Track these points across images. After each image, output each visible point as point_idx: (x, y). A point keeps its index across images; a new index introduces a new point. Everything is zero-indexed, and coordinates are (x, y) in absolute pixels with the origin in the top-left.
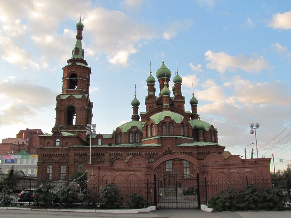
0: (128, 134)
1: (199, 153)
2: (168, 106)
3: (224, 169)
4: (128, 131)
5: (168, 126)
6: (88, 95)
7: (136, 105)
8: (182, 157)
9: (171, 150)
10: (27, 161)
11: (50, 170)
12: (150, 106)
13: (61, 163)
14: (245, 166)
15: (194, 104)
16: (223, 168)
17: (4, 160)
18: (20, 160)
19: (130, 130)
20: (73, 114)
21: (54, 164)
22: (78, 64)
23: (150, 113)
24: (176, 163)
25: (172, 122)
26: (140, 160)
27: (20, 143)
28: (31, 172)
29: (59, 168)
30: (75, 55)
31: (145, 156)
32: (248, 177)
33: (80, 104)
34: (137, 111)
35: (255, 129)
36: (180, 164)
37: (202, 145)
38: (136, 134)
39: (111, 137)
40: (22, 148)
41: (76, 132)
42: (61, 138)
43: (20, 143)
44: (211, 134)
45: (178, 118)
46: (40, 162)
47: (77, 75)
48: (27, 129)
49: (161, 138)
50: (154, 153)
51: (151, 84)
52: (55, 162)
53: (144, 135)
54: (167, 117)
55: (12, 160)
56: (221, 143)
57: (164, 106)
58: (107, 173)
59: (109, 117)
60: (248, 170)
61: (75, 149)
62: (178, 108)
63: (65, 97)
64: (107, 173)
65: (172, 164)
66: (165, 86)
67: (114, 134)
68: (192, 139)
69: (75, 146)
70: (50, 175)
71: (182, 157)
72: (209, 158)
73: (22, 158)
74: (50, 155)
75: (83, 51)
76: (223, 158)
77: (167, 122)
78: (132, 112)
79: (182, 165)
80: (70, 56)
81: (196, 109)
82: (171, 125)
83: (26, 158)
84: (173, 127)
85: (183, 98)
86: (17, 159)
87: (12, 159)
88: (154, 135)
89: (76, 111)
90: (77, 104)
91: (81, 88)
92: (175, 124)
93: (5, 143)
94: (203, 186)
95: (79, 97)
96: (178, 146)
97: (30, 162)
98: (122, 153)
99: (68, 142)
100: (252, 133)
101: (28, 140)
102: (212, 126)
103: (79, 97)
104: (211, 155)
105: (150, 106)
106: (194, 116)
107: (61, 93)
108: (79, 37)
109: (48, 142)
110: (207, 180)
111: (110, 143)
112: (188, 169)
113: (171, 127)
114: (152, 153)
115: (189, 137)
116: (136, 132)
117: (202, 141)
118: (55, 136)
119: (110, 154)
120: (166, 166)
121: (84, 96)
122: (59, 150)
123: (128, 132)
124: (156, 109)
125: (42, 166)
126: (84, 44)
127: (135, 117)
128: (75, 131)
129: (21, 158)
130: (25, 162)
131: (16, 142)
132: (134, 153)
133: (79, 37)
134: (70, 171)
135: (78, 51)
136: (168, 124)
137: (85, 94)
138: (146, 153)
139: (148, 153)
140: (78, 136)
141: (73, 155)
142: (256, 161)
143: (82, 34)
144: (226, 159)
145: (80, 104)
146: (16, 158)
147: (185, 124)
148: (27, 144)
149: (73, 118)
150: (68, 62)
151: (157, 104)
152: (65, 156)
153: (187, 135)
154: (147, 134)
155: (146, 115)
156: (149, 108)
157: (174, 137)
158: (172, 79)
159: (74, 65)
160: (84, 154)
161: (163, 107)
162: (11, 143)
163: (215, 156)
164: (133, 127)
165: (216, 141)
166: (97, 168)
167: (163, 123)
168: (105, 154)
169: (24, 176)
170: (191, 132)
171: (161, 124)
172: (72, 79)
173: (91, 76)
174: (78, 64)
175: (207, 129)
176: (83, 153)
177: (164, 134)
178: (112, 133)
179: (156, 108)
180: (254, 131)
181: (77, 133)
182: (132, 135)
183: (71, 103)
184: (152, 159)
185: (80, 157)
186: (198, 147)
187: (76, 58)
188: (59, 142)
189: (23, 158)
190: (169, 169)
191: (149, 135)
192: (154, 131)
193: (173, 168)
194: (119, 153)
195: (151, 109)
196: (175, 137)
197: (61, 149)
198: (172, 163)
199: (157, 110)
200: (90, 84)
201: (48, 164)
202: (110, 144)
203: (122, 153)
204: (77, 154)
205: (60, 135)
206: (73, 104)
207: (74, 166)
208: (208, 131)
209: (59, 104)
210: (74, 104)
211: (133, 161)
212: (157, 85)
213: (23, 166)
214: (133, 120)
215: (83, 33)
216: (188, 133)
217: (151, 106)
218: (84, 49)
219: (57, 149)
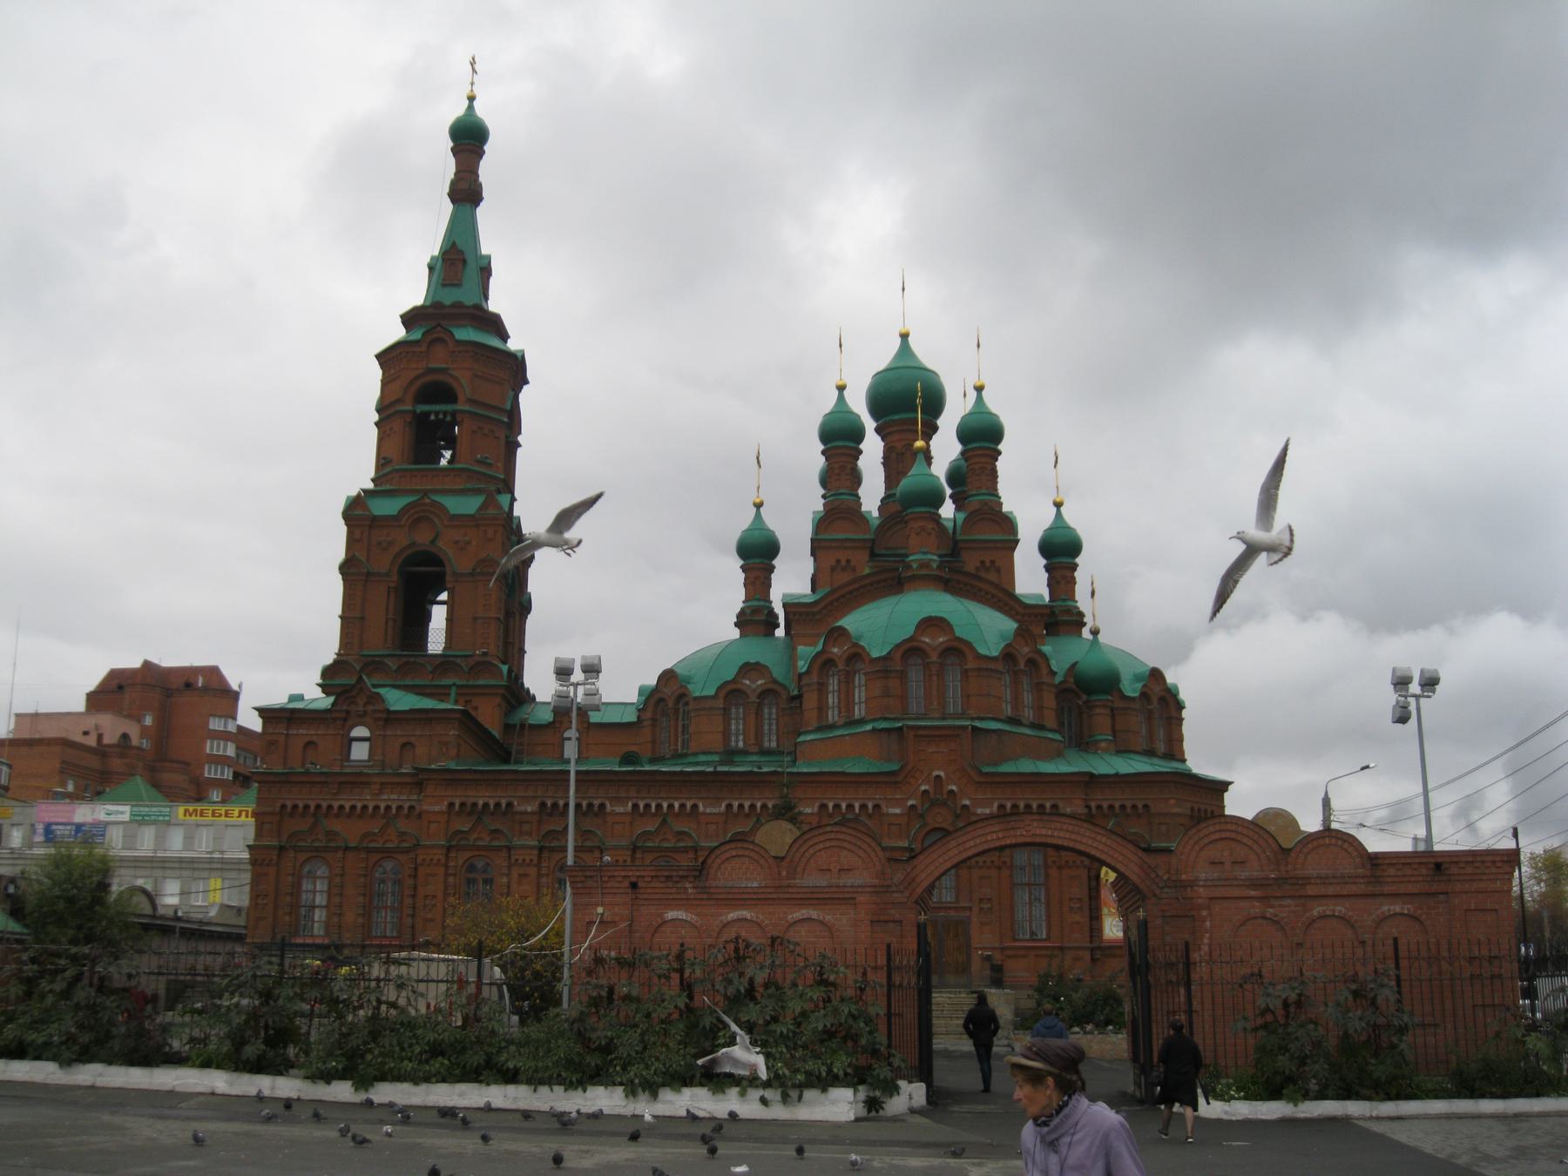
0: (720, 703)
2: (935, 565)
3: (1276, 903)
4: (719, 689)
6: (513, 499)
7: (758, 554)
8: (1062, 834)
9: (952, 791)
10: (160, 840)
11: (318, 888)
12: (838, 561)
13: (376, 850)
14: (1387, 889)
15: (1061, 551)
16: (1276, 897)
17: (40, 828)
18: (121, 827)
19: (733, 686)
20: (430, 597)
21: (340, 854)
22: (465, 334)
23: (837, 600)
25: (958, 650)
26: (845, 845)
27: (106, 741)
28: (182, 894)
29: (362, 880)
30: (444, 285)
33: (469, 543)
34: (767, 585)
35: (1417, 697)
36: (999, 868)
37: (1112, 772)
38: (760, 706)
39: (634, 719)
40: (116, 764)
41: (453, 691)
42: (376, 720)
43: (106, 741)
44: (1150, 712)
45: (988, 629)
46: (268, 847)
47: (450, 386)
48: (147, 664)
49: (901, 728)
50: (863, 807)
51: (839, 439)
52: (347, 849)
53: (810, 715)
54: (933, 624)
55: (79, 827)
56: (1199, 762)
57: (915, 566)
58: (671, 915)
59: (624, 610)
60: (1398, 909)
61: (451, 779)
62: (983, 574)
63: (387, 507)
64: (671, 915)
66: (920, 457)
67: (646, 702)
68: (1057, 737)
69: (453, 766)
70: (318, 915)
71: (1062, 834)
72: (1202, 843)
73: (131, 821)
74: (318, 807)
75: (484, 263)
76: (1274, 845)
77: (933, 649)
78: (740, 594)
80: (415, 293)
81: (1073, 581)
83: (155, 823)
84: (965, 673)
85: (1007, 524)
86: (108, 823)
87: (83, 825)
88: (858, 712)
89: (448, 578)
90: (457, 542)
91: (479, 462)
93: (26, 736)
94: (1169, 982)
95: (466, 505)
96: (988, 774)
97: (204, 845)
98: (695, 806)
99: (412, 740)
100: (1402, 718)
101: (148, 721)
102: (1156, 675)
103: (466, 505)
104: (1212, 829)
105: (838, 561)
106: (1060, 617)
107: (370, 486)
108: (466, 193)
109: (404, 740)
110: (1195, 956)
111: (634, 748)
113: (953, 680)
114: (850, 807)
115: (1042, 727)
116: (764, 694)
117: (1106, 750)
118: (348, 712)
119: (635, 806)
121: (490, 502)
122: (368, 783)
123: (723, 692)
124: (868, 575)
125: (272, 859)
126: (493, 234)
127: (755, 619)
128: (449, 687)
129: (126, 817)
130: (146, 843)
131: (86, 733)
132: (759, 805)
133: (466, 193)
134: (426, 897)
135: (459, 264)
137: (499, 492)
139: (831, 805)
140: (465, 713)
141: (440, 812)
142: (1438, 866)
143: (480, 172)
144: (1286, 851)
145: (469, 543)
146: (102, 817)
147: (1019, 662)
148: (145, 744)
149: (427, 617)
150: (409, 319)
151: (873, 555)
152: (397, 816)
153: (1028, 714)
154: (822, 708)
155: (815, 610)
156: (833, 569)
157: (964, 728)
158: (949, 422)
159: (439, 340)
160: (498, 805)
161: (908, 566)
162: (63, 735)
163: (1233, 835)
164: (748, 669)
165: (1174, 750)
166: (626, 884)
167: (910, 650)
168: (609, 808)
169: (154, 917)
170: (1050, 701)
171: (898, 655)
172: (427, 414)
173: (526, 397)
174: (465, 334)
175: (1130, 688)
176: (492, 803)
177: (914, 708)
178: (633, 697)
179: (867, 571)
180: (1413, 708)
181: (458, 694)
183: (423, 538)
185: (479, 818)
186: (1090, 781)
187: (448, 302)
188: (366, 745)
189: (139, 821)
191: (833, 715)
192: (859, 694)
194: (683, 806)
195: (844, 578)
196: (974, 729)
197: (375, 779)
199: (871, 584)
200: (520, 438)
201: (302, 857)
202: (628, 759)
203: (695, 806)
204: (463, 805)
205: (370, 708)
206: (433, 542)
207: (447, 867)
208: (1133, 699)
209: (359, 541)
210: (440, 544)
211: (811, 851)
212: (872, 448)
213: (136, 860)
214: (742, 635)
215: (488, 171)
216: (1039, 708)
217: (843, 563)
218: (489, 258)
219: (356, 780)
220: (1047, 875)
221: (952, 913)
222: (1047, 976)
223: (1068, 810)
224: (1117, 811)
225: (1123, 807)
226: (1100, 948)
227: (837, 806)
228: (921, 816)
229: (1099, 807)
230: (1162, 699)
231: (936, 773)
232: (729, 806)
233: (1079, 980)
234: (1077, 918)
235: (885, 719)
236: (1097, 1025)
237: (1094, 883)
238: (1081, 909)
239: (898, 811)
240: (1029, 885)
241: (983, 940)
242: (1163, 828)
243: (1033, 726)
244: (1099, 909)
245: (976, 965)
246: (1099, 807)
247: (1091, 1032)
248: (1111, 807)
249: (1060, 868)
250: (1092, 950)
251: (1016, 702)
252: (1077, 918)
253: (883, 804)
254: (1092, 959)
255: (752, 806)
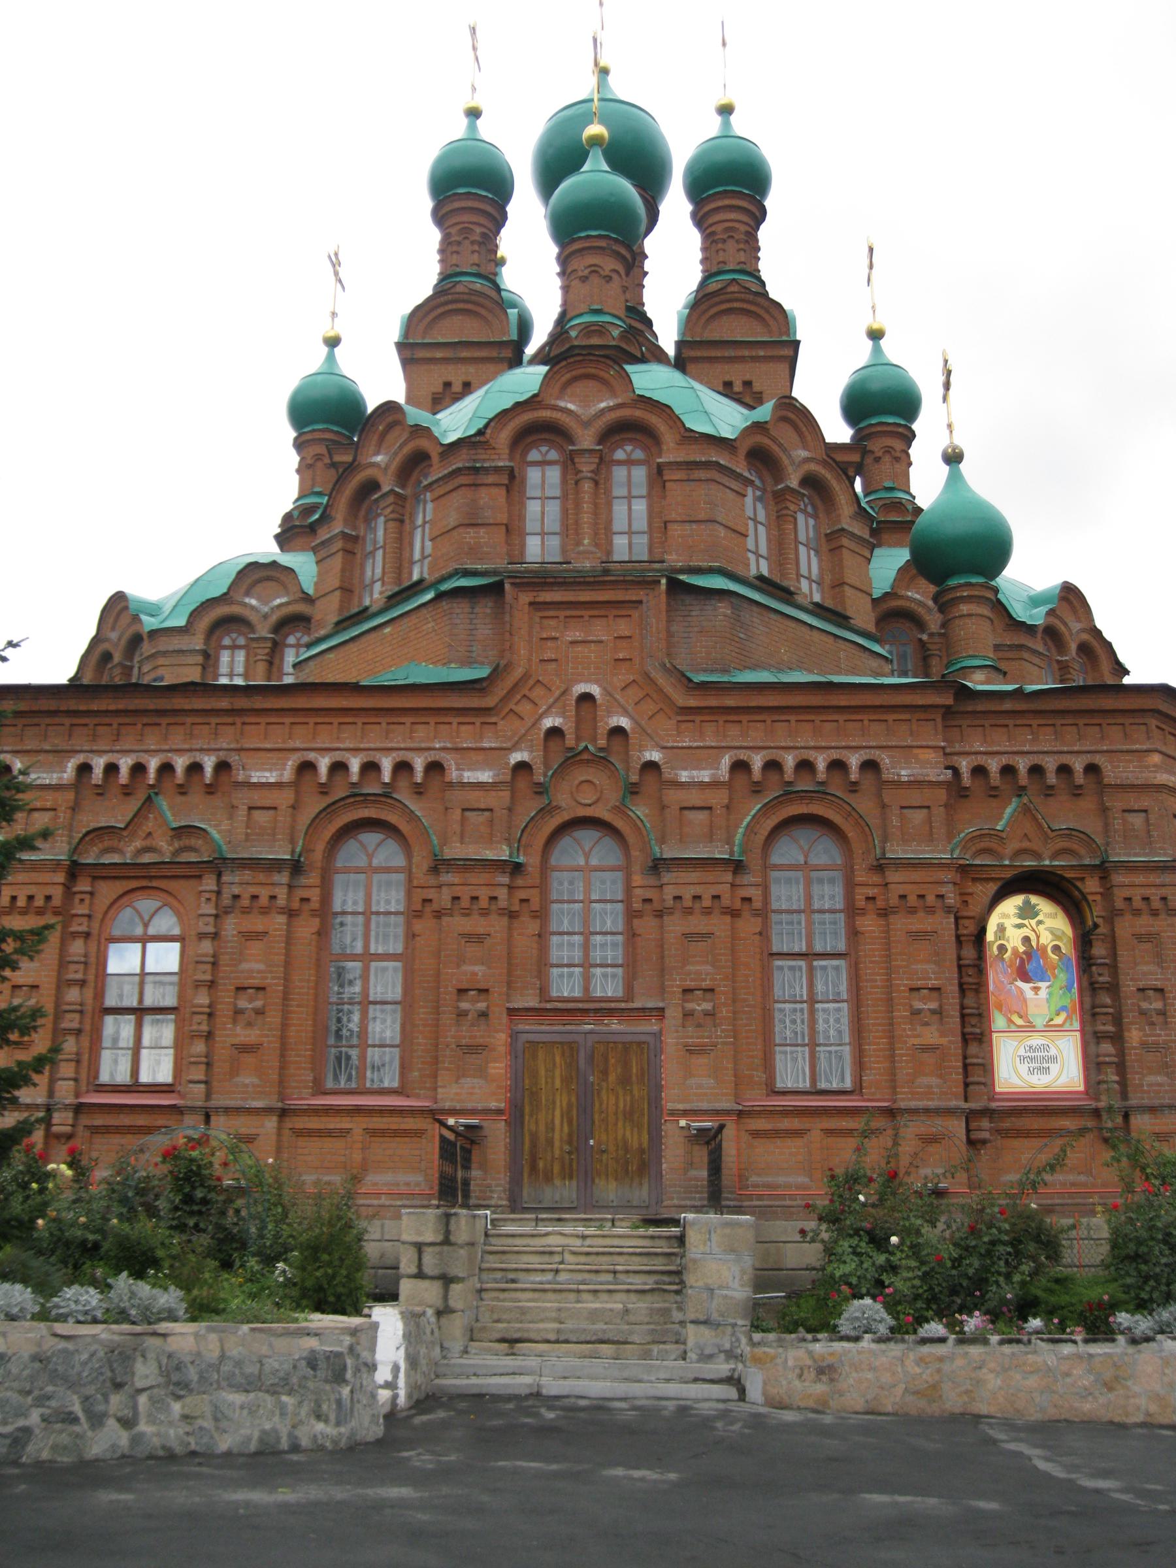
1: (966, 780)
2: (616, 333)
4: (195, 614)
5: (586, 466)
9: (618, 731)
24: (669, 892)
31: (285, 798)
32: (942, 1345)
36: (734, 914)
50: (403, 767)
57: (573, 334)
65: (631, 915)
79: (749, 925)
82: (629, 462)
84: (658, 475)
92: (669, 438)
96: (704, 686)
112: (833, 979)
113: (630, 480)
114: (370, 767)
120: (542, 937)
132: (153, 764)
136: (586, 440)
138: (307, 767)
139: (324, 764)
171: (504, 437)
182: (241, 656)
184: (371, 838)
190: (587, 965)
192: (420, 544)
193: (631, 966)
198: (627, 900)
208: (1030, 629)
220: (854, 934)
221: (615, 1025)
222: (854, 1180)
223: (905, 774)
224: (1023, 777)
225: (1036, 770)
226: (987, 1113)
227: (339, 767)
228: (540, 790)
229: (979, 771)
230: (1084, 649)
231: (581, 688)
232: (84, 769)
233: (939, 1193)
234: (931, 1035)
235: (467, 573)
236: (994, 1316)
237: (969, 953)
238: (939, 1012)
239: (485, 776)
240: (808, 955)
241: (693, 1088)
242: (1137, 820)
243: (819, 610)
244: (982, 1016)
245: (674, 1151)
246: (979, 771)
247: (979, 1339)
248: (1008, 771)
249: (884, 913)
250: (971, 1116)
251: (781, 549)
252: (931, 1035)
253: (450, 762)
254: (971, 1142)
255: (139, 769)
